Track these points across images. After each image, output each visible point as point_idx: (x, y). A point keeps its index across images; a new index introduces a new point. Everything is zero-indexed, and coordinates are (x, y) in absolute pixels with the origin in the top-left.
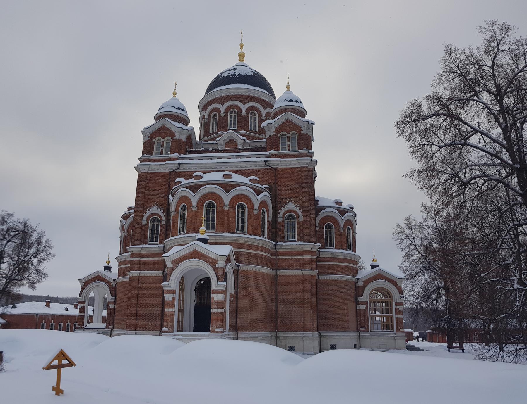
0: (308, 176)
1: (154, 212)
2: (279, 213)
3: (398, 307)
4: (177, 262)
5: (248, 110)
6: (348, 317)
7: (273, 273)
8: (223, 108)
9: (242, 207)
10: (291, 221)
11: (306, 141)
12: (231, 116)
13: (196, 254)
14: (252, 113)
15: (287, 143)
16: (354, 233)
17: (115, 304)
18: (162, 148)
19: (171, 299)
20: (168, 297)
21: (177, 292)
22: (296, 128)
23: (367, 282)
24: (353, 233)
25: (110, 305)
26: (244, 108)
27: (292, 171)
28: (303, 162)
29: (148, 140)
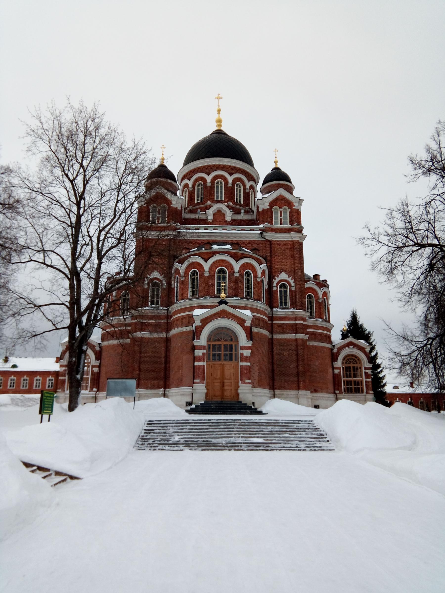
0: (296, 250)
1: (155, 276)
2: (274, 282)
5: (234, 181)
6: (182, 371)
7: (270, 337)
8: (209, 179)
9: (248, 274)
10: (283, 289)
11: (296, 217)
12: (217, 187)
13: (227, 315)
14: (237, 185)
15: (280, 218)
16: (329, 304)
18: (281, 217)
22: (289, 204)
23: (341, 348)
24: (327, 304)
25: (94, 369)
26: (230, 179)
27: (284, 243)
28: (294, 237)
29: (267, 209)
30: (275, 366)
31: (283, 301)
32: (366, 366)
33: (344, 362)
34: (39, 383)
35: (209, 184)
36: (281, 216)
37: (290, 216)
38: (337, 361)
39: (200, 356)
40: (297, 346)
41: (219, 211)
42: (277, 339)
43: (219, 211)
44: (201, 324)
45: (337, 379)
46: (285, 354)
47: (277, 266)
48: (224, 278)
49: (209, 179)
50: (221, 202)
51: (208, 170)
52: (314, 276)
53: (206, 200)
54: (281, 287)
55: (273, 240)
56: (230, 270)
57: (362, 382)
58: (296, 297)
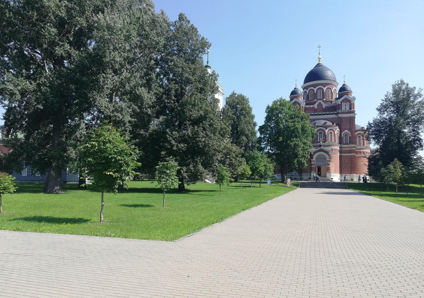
8: (315, 90)
9: (331, 133)
11: (352, 106)
22: (349, 101)
27: (347, 118)
28: (351, 115)
35: (315, 92)
40: (351, 158)
41: (320, 103)
43: (320, 103)
47: (343, 127)
48: (322, 135)
49: (315, 90)
50: (320, 99)
51: (315, 86)
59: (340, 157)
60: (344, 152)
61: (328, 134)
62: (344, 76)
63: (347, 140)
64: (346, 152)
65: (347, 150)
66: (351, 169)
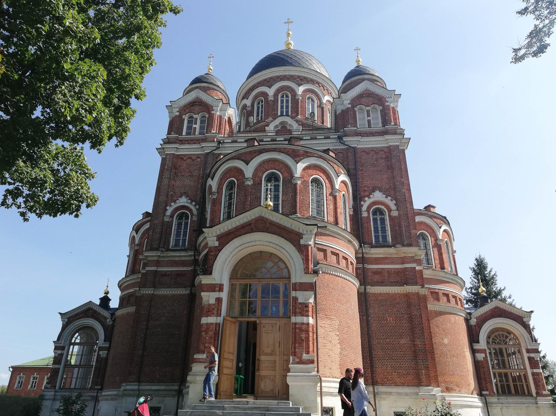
2: (362, 206)
3: (532, 355)
4: (225, 239)
8: (271, 92)
10: (378, 217)
12: (282, 102)
14: (309, 98)
17: (109, 351)
18: (369, 118)
19: (212, 301)
20: (208, 298)
21: (226, 288)
25: (101, 353)
27: (375, 151)
28: (391, 140)
30: (375, 342)
31: (380, 234)
32: (529, 347)
33: (491, 340)
34: (36, 382)
35: (271, 98)
36: (369, 115)
37: (381, 116)
38: (478, 342)
39: (209, 305)
40: (409, 306)
42: (374, 295)
44: (217, 244)
45: (482, 370)
46: (390, 319)
47: (367, 182)
52: (425, 208)
53: (267, 116)
54: (375, 213)
55: (358, 147)
56: (286, 175)
57: (526, 376)
58: (400, 227)
59: (364, 299)
60: (377, 278)
61: (305, 183)
62: (357, 49)
63: (384, 230)
64: (384, 278)
65: (389, 271)
66: (415, 357)
